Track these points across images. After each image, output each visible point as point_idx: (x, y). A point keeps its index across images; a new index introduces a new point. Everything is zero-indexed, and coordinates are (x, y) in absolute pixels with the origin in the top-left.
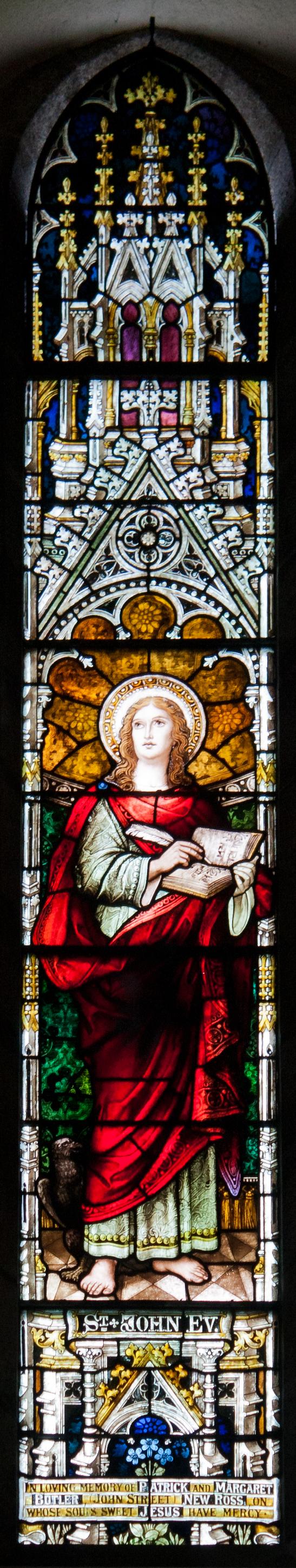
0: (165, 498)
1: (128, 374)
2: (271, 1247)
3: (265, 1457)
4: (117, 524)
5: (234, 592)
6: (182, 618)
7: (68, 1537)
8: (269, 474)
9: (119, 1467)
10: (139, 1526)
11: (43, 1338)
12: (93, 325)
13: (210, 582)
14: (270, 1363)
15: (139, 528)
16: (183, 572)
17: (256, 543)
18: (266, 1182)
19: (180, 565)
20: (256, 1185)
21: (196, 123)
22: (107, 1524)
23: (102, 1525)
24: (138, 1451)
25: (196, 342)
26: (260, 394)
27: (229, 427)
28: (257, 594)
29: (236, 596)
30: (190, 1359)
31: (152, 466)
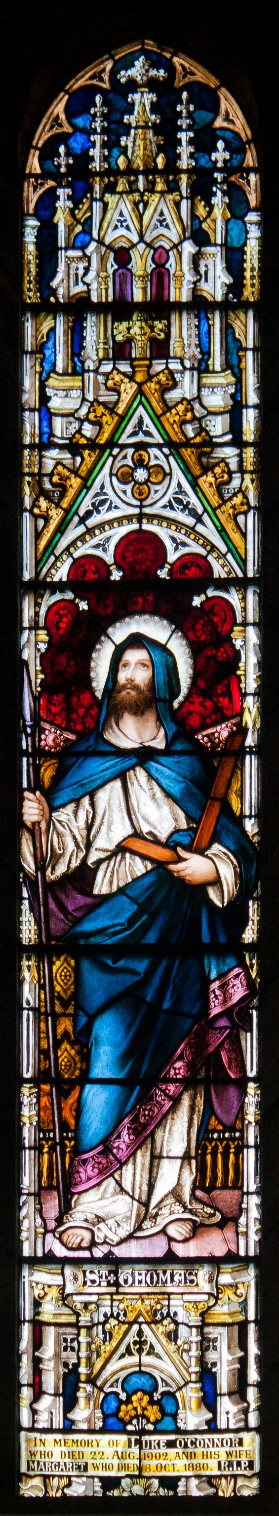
0: (129, 1190)
1: (119, 309)
2: (254, 1200)
3: (246, 1411)
4: (111, 459)
5: (222, 531)
6: (172, 557)
7: (66, 1491)
8: (255, 407)
9: (112, 1423)
10: (128, 1480)
11: (42, 1292)
12: (87, 270)
13: (199, 520)
14: (251, 1316)
15: (131, 464)
16: (172, 508)
17: (243, 480)
18: (251, 1135)
19: (170, 502)
20: (242, 1138)
21: (185, 95)
22: (102, 1479)
23: (96, 1480)
24: (130, 1407)
25: (185, 283)
26: (247, 329)
27: (217, 361)
28: (244, 535)
29: (223, 533)
30: (175, 1314)
31: (143, 399)
